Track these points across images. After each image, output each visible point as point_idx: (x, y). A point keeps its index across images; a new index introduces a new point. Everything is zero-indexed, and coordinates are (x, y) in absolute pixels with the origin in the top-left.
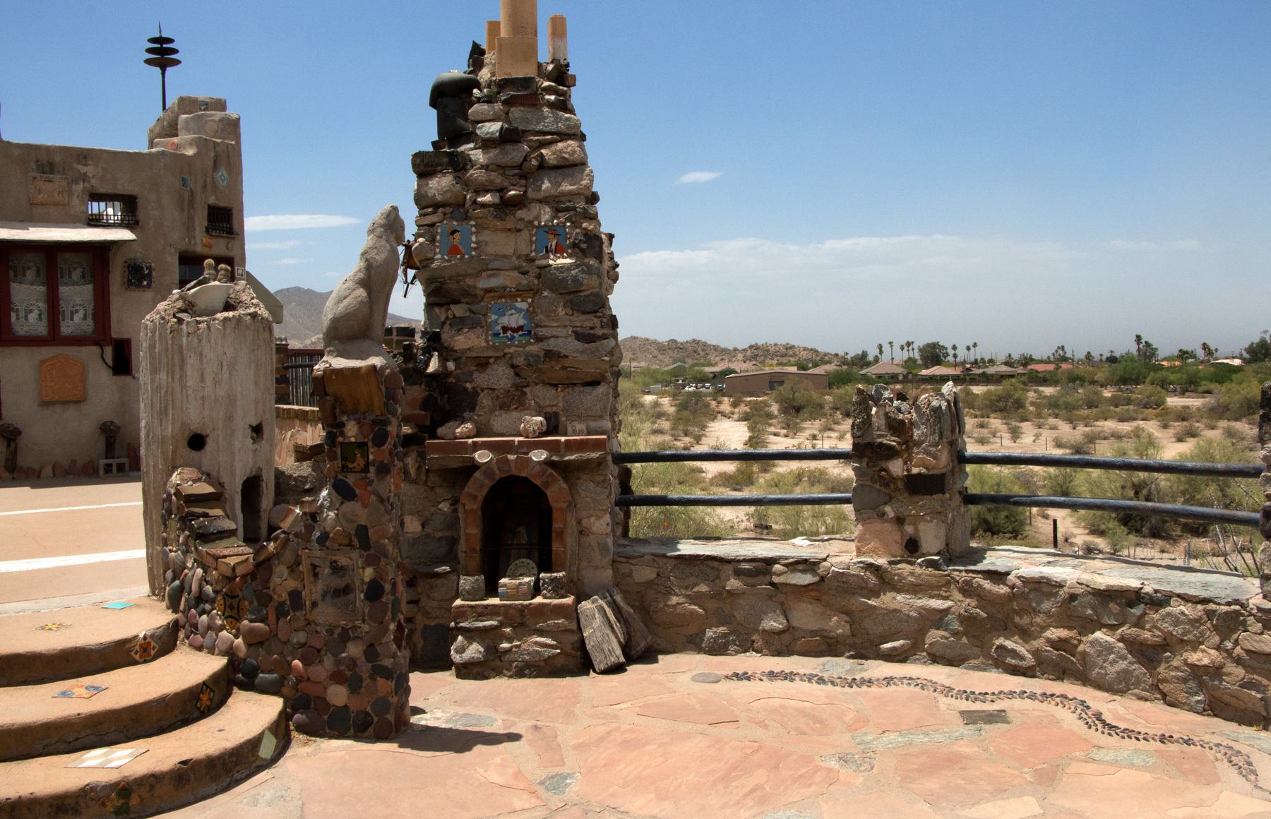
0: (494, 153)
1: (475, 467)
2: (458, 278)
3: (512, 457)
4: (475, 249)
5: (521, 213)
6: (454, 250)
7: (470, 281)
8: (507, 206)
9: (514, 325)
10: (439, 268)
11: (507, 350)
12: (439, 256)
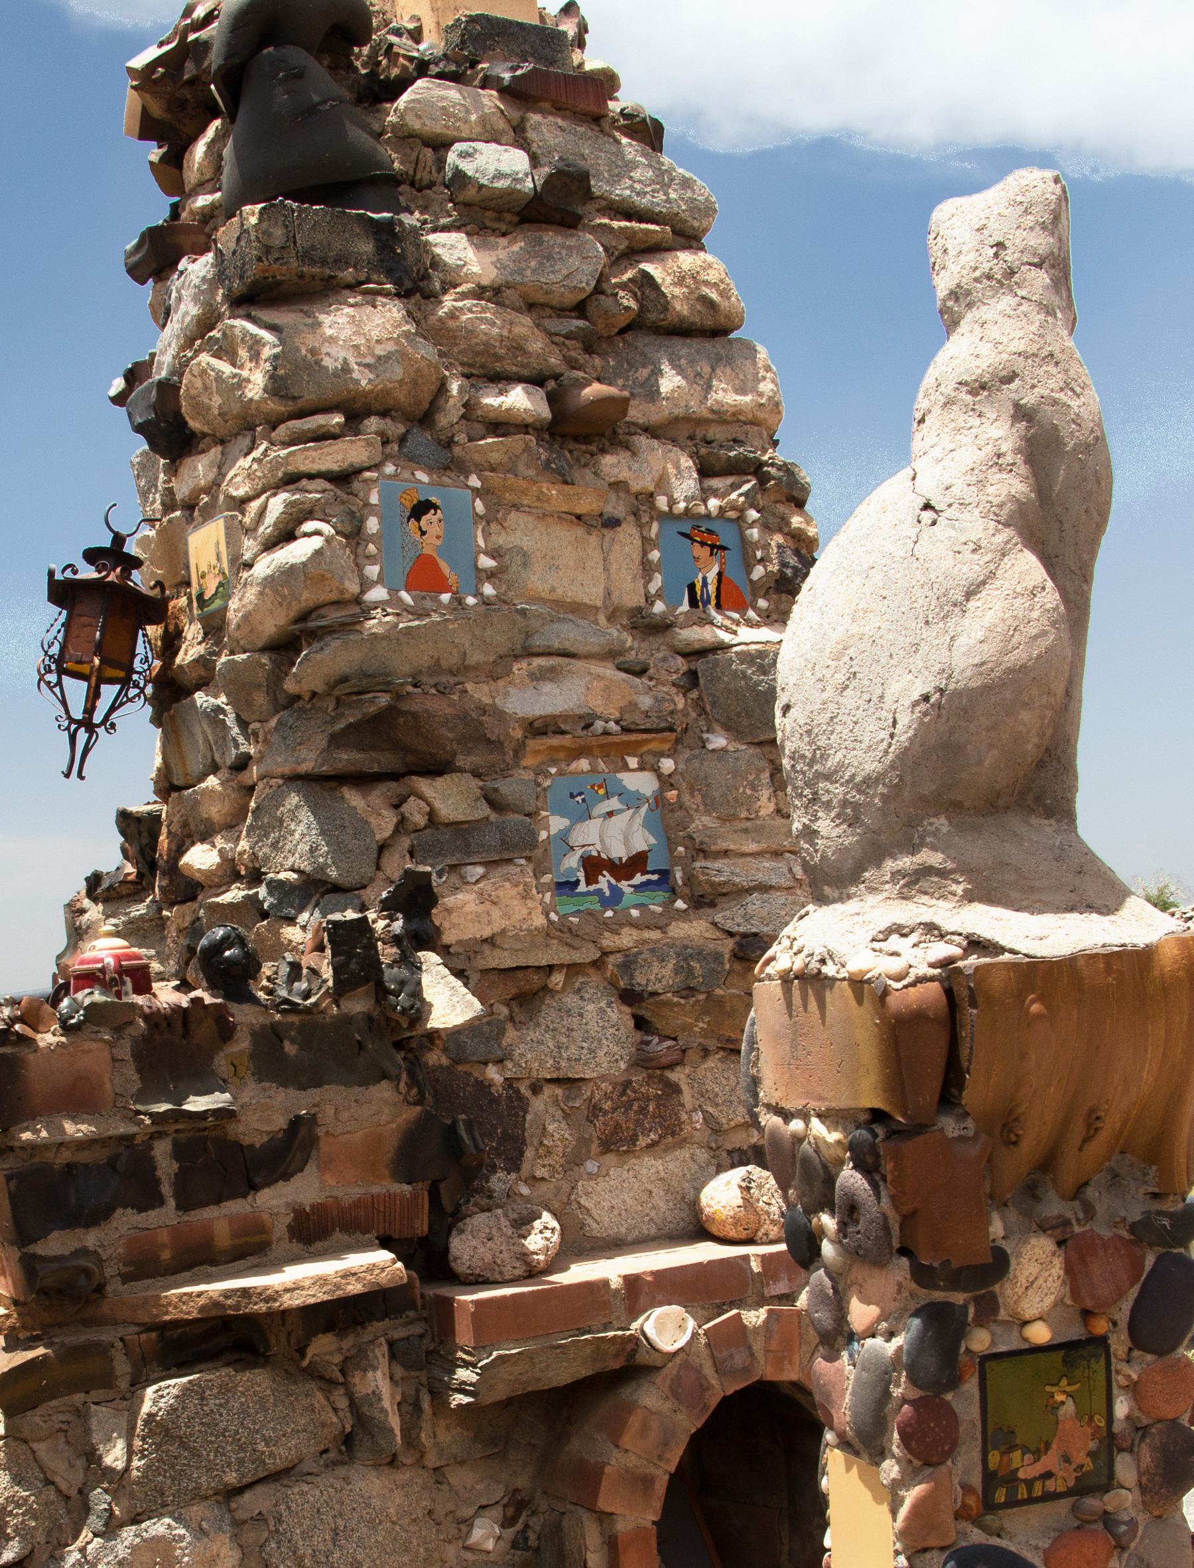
0: (509, 249)
1: (633, 1365)
2: (448, 676)
3: (755, 1317)
4: (491, 575)
5: (613, 464)
6: (424, 576)
7: (479, 692)
8: (577, 433)
9: (619, 852)
10: (391, 636)
11: (608, 941)
12: (378, 594)
